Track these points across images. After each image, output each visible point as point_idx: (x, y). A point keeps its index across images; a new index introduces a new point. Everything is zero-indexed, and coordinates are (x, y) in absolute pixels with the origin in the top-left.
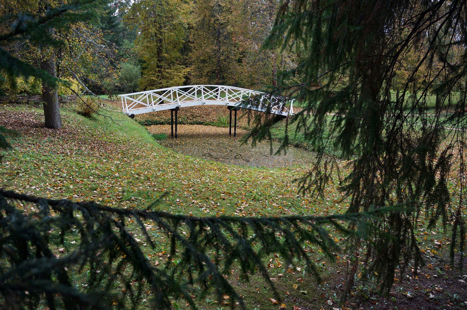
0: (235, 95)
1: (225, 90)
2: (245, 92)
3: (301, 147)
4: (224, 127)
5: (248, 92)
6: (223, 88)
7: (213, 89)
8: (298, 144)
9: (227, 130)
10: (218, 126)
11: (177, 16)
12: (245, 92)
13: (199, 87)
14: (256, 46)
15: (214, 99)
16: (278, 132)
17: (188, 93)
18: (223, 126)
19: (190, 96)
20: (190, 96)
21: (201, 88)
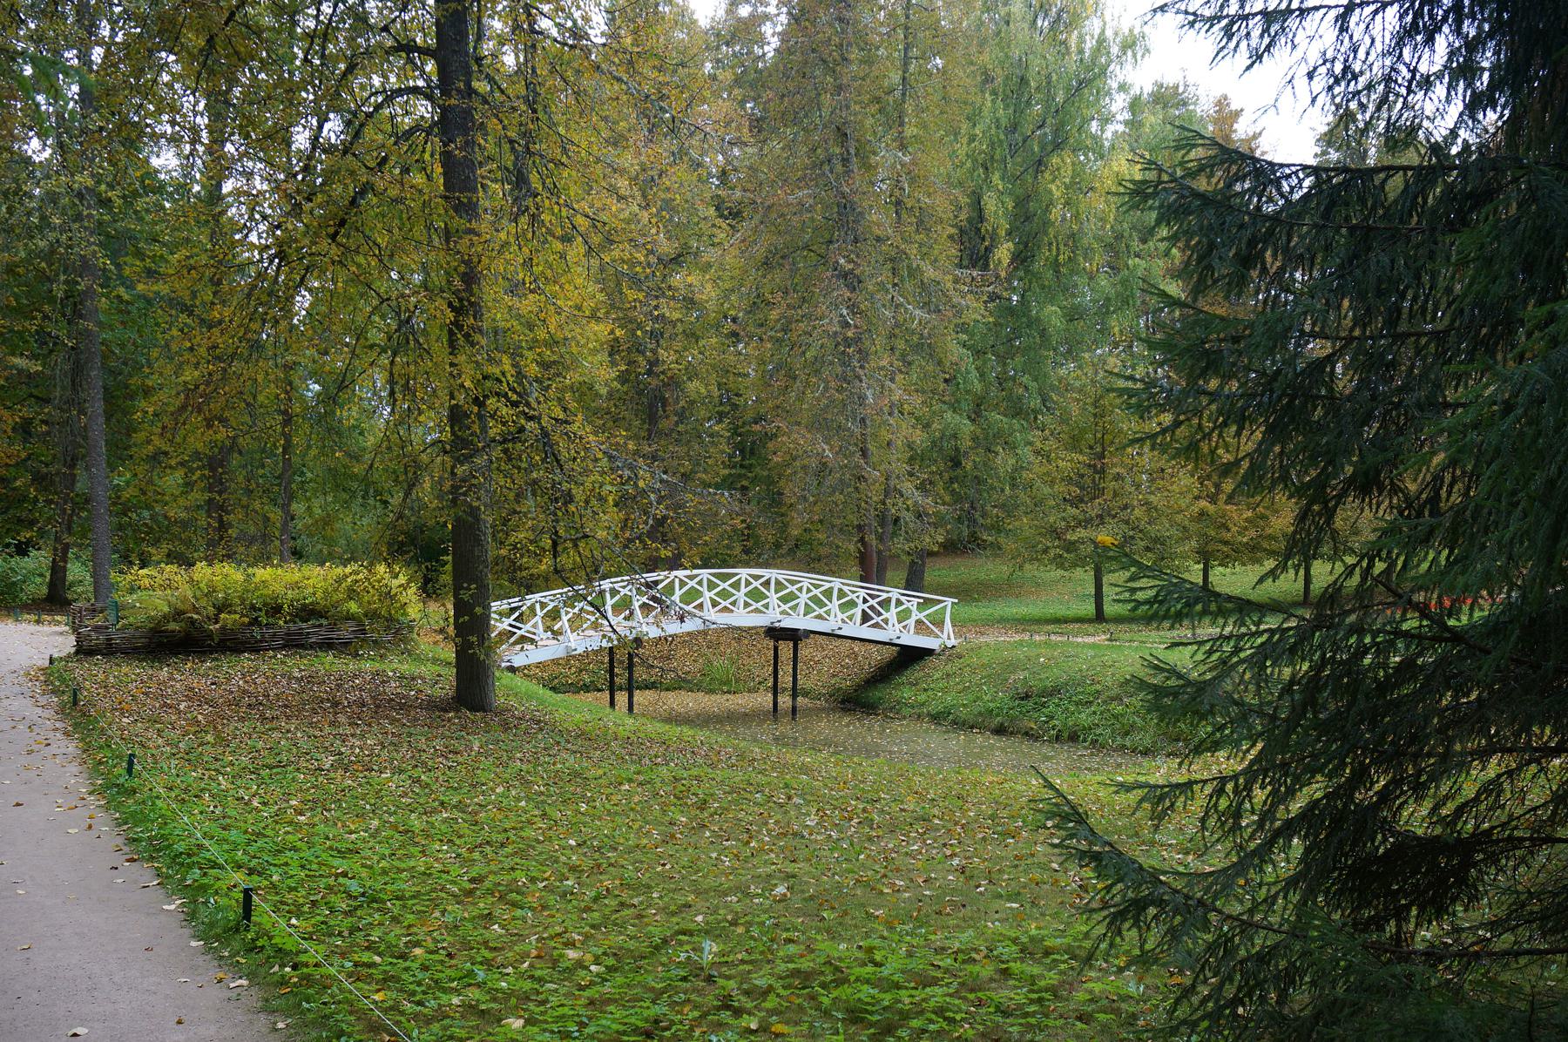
0: (787, 602)
1: (767, 584)
2: (817, 587)
3: (1012, 733)
4: (729, 692)
5: (827, 585)
6: (757, 578)
7: (673, 589)
8: (1002, 724)
9: (764, 700)
10: (711, 692)
11: (575, 362)
12: (817, 587)
13: (691, 578)
14: (826, 447)
15: (761, 612)
16: (922, 697)
17: (730, 585)
18: (725, 688)
19: (520, 629)
20: (520, 629)
21: (700, 583)
